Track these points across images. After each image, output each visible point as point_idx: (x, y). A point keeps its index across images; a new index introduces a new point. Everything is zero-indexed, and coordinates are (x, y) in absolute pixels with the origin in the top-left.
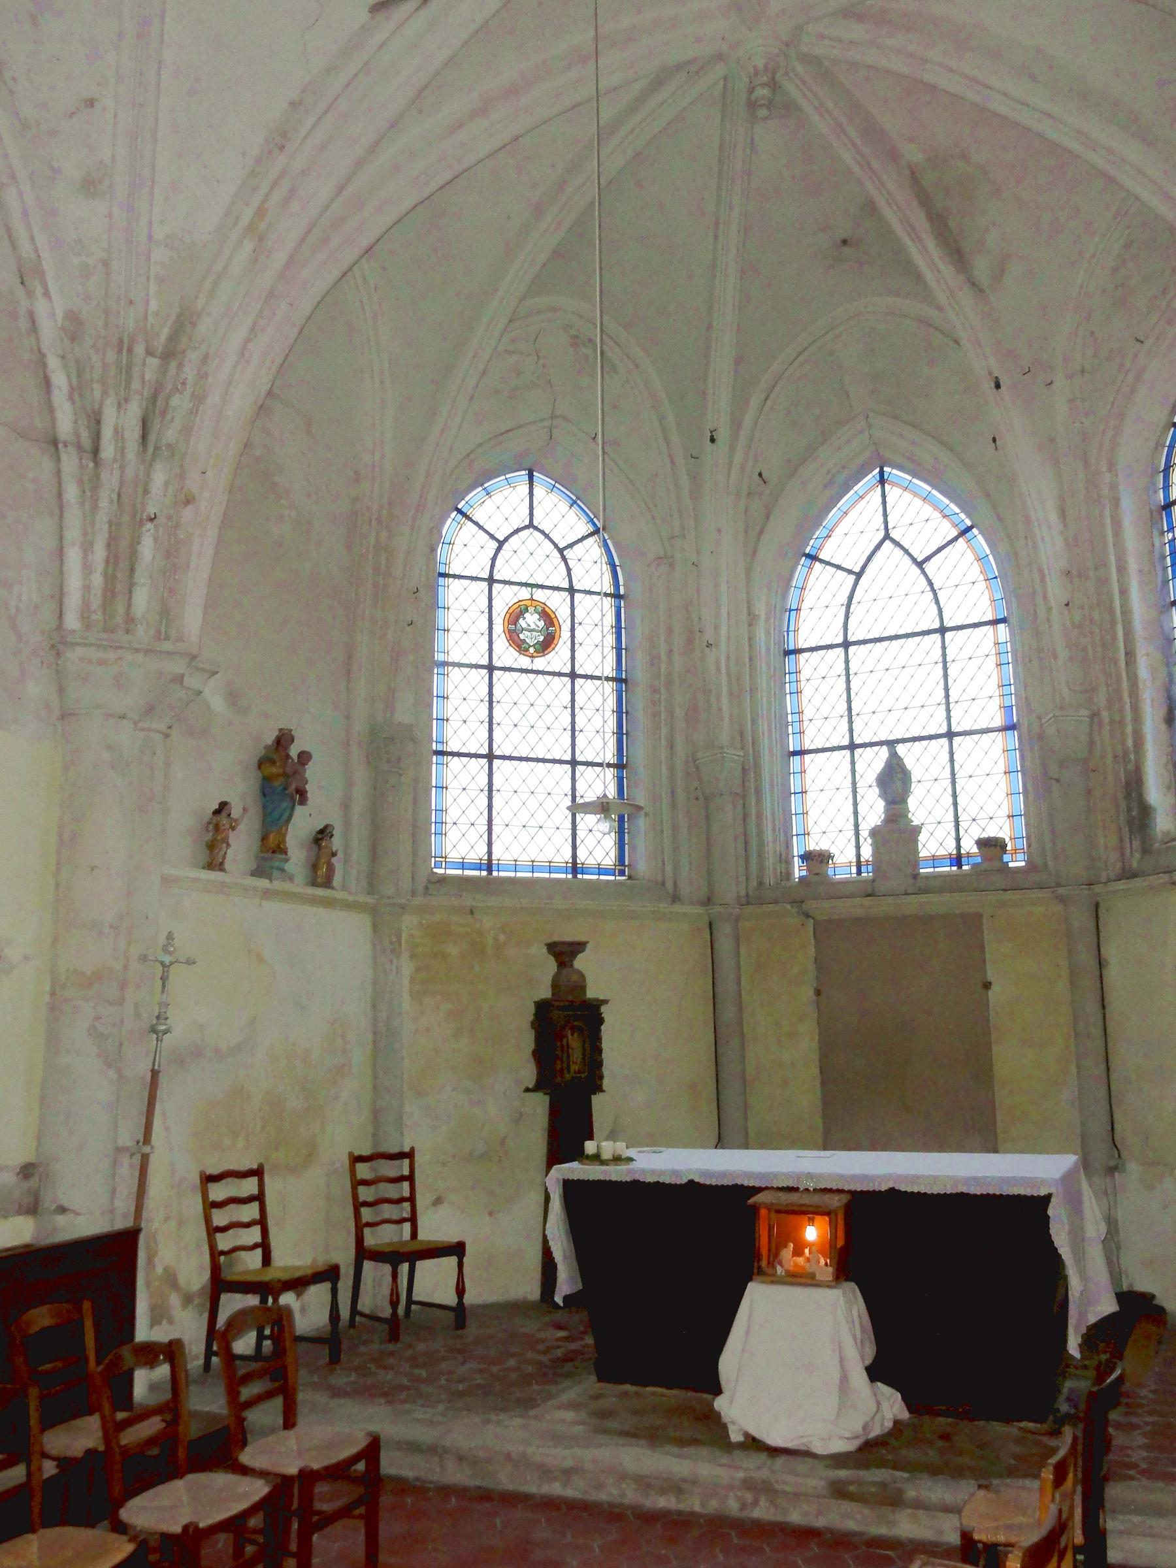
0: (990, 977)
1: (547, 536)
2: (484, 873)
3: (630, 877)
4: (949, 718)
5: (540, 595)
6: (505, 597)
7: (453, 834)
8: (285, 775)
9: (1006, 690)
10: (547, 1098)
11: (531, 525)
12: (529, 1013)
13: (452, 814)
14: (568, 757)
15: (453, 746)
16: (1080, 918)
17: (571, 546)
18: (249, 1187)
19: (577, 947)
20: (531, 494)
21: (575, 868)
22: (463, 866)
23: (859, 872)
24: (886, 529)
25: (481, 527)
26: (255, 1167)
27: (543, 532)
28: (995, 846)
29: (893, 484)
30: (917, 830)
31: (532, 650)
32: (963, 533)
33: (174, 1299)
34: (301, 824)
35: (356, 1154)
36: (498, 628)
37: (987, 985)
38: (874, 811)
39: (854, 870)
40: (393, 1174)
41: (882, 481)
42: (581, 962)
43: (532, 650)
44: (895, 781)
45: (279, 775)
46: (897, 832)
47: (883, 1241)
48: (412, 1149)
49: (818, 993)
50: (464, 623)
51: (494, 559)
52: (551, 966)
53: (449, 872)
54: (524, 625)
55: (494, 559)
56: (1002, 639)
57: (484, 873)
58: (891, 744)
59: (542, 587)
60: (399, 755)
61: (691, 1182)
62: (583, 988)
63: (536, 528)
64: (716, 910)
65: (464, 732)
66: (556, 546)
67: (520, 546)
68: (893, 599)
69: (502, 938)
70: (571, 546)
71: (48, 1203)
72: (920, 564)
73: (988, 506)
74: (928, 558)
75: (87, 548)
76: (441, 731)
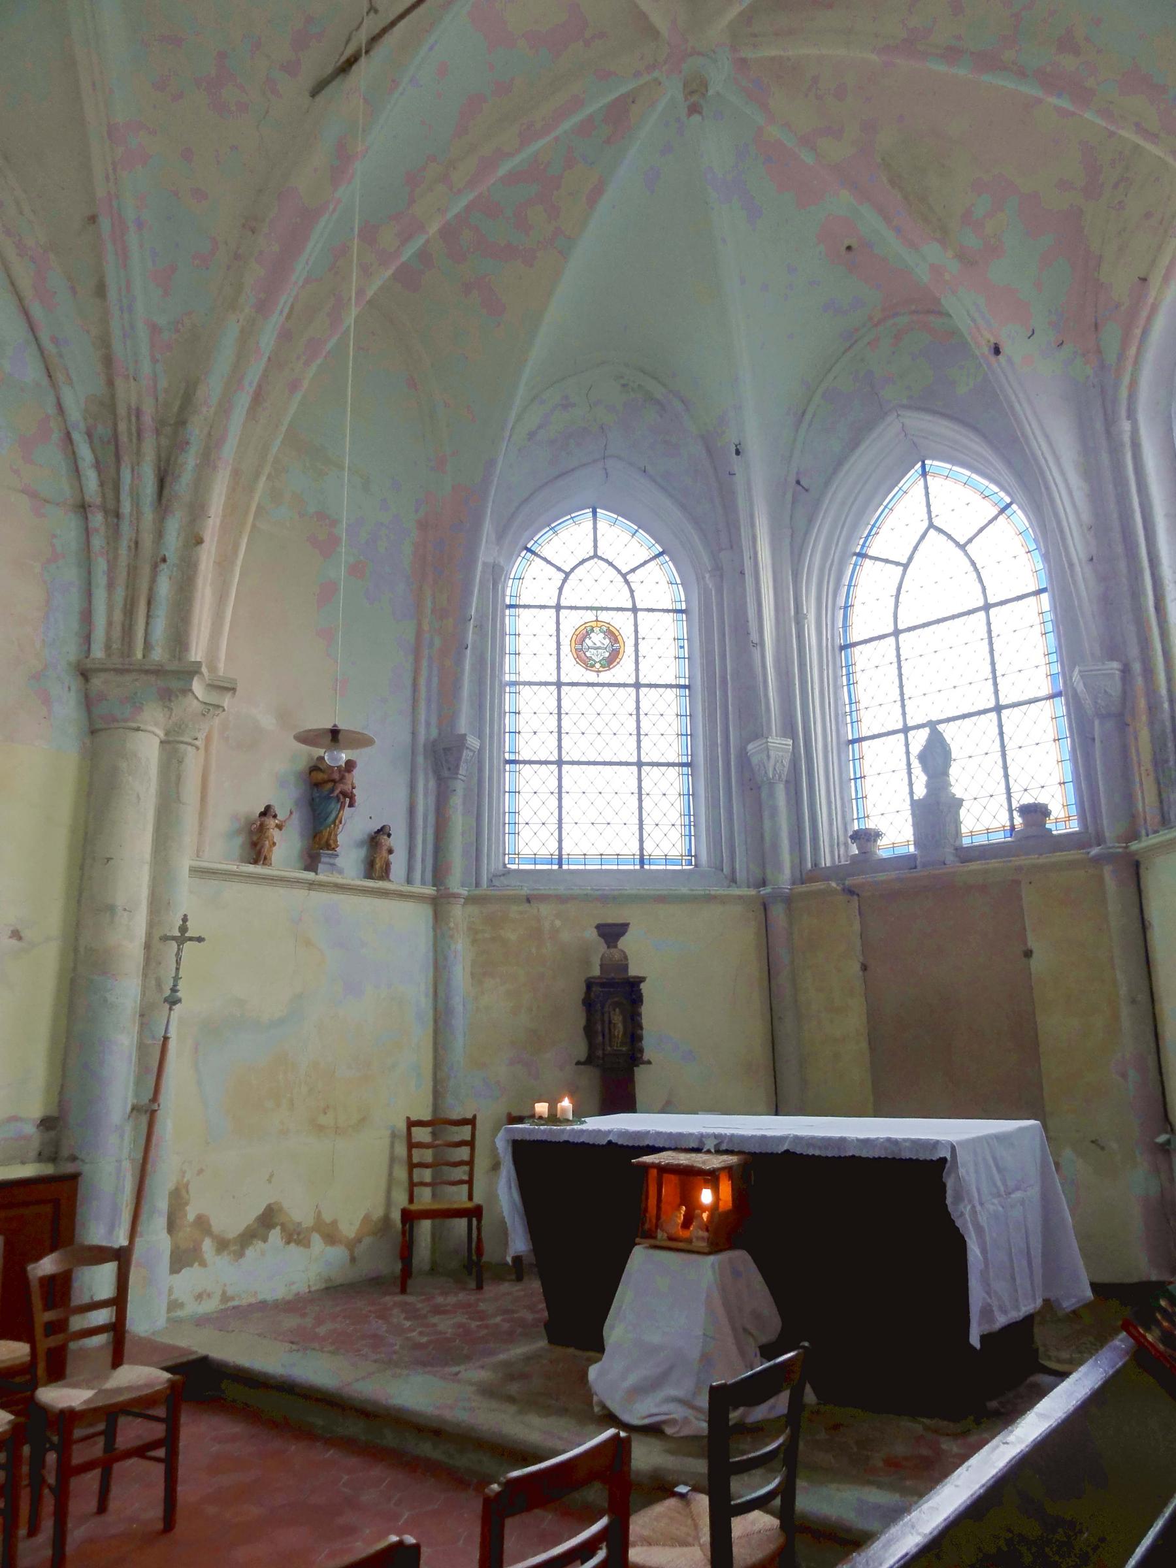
0: (1032, 943)
1: (611, 564)
2: (556, 867)
3: (696, 866)
4: (996, 692)
5: (604, 616)
6: (571, 622)
7: (525, 833)
11: (596, 556)
12: (579, 993)
13: (525, 815)
14: (635, 759)
15: (525, 755)
17: (633, 570)
24: (930, 518)
25: (549, 562)
27: (606, 561)
28: (1036, 811)
29: (935, 475)
30: (959, 803)
31: (598, 665)
32: (1002, 511)
33: (207, 1245)
34: (352, 827)
35: (414, 1118)
36: (566, 649)
37: (1028, 954)
41: (924, 474)
43: (598, 665)
44: (936, 757)
46: (936, 812)
48: (475, 1117)
49: (864, 968)
50: (531, 645)
51: (561, 589)
53: (522, 867)
54: (590, 644)
55: (561, 589)
57: (556, 867)
59: (607, 609)
60: (456, 761)
61: (610, 1142)
64: (767, 890)
65: (535, 741)
66: (619, 571)
68: (940, 582)
69: (558, 923)
70: (633, 570)
71: (65, 1153)
72: (963, 547)
73: (1026, 482)
74: (970, 541)
75: (111, 586)
76: (514, 743)
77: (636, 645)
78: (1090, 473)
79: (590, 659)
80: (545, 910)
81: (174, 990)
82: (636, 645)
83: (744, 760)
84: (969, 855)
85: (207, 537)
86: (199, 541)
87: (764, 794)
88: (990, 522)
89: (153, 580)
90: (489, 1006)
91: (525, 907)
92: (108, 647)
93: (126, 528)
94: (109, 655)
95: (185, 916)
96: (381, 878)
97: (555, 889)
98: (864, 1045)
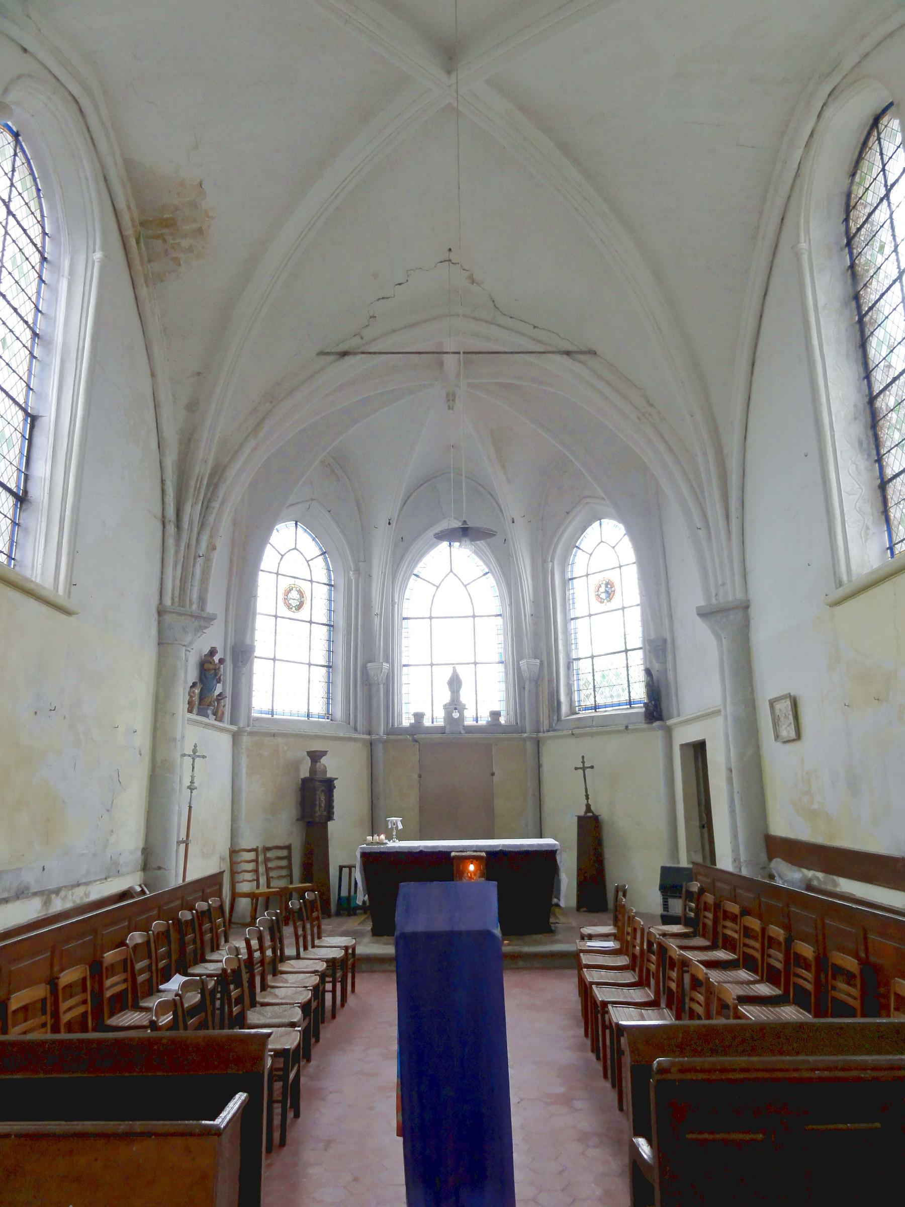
0: (494, 770)
6: (285, 583)
8: (215, 670)
10: (779, 860)
18: (284, 853)
19: (324, 753)
26: (287, 844)
37: (493, 774)
38: (444, 696)
42: (324, 760)
44: (455, 683)
46: (455, 705)
49: (420, 776)
50: (267, 592)
62: (325, 772)
67: (292, 559)
69: (286, 748)
72: (465, 586)
75: (175, 566)
78: (534, 577)
80: (280, 740)
81: (192, 782)
83: (364, 668)
84: (469, 730)
85: (219, 545)
86: (214, 548)
87: (374, 689)
89: (194, 566)
90: (257, 790)
92: (173, 599)
93: (185, 536)
96: (221, 720)
97: (274, 732)
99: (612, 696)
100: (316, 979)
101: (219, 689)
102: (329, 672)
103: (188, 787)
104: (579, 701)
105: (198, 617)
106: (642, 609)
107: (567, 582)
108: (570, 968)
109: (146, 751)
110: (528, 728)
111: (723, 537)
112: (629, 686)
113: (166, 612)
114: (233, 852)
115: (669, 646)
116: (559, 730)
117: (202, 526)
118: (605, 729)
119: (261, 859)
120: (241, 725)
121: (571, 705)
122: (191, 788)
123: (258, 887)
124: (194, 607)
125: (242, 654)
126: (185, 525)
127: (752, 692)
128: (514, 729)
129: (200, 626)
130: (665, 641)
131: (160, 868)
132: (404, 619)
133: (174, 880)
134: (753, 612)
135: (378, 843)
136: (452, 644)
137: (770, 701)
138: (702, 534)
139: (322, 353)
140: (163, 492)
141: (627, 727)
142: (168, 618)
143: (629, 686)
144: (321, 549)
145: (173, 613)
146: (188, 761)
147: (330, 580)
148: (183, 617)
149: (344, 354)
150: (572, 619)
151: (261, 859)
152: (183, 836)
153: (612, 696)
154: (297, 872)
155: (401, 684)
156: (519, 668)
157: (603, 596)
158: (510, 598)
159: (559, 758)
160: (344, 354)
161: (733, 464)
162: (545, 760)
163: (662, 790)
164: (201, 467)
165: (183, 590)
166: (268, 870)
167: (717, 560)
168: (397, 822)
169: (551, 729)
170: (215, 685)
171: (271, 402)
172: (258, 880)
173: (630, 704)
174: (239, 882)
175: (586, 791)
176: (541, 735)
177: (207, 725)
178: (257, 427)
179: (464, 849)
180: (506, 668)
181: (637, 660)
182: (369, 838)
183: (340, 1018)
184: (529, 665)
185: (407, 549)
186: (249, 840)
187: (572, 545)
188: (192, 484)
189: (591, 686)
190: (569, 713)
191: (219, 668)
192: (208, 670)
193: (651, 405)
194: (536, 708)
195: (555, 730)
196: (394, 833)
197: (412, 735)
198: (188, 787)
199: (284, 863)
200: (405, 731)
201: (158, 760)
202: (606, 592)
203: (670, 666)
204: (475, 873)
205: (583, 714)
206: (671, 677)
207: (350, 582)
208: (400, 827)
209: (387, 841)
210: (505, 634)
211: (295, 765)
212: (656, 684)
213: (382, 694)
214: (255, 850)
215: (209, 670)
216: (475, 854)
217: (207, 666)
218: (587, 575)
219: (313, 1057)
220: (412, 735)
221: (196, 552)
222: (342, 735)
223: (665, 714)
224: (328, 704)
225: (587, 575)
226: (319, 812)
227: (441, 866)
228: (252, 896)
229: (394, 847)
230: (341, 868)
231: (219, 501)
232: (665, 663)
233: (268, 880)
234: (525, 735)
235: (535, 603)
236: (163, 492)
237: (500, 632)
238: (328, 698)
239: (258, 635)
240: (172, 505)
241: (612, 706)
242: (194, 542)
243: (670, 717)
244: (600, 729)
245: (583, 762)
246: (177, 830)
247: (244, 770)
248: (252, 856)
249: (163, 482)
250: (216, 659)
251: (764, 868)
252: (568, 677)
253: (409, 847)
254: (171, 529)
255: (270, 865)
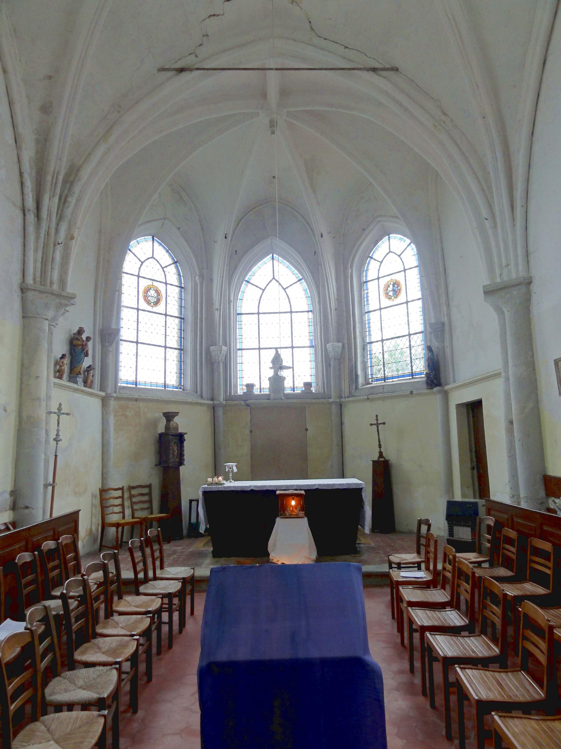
2: (134, 386)
5: (155, 284)
6: (144, 284)
8: (83, 345)
9: (311, 334)
11: (153, 257)
16: (334, 409)
17: (166, 267)
18: (146, 491)
19: (177, 414)
20: (153, 246)
21: (165, 386)
22: (127, 383)
23: (260, 392)
26: (148, 484)
31: (393, 298)
35: (131, 485)
37: (307, 430)
39: (259, 390)
40: (116, 496)
41: (273, 259)
42: (176, 419)
43: (393, 298)
45: (80, 345)
46: (277, 381)
47: (317, 505)
48: (123, 487)
49: (251, 432)
50: (129, 291)
51: (140, 268)
52: (164, 421)
55: (140, 268)
56: (310, 317)
57: (134, 386)
58: (276, 349)
62: (177, 428)
63: (154, 259)
67: (147, 263)
68: (274, 299)
69: (146, 410)
70: (166, 267)
72: (285, 289)
74: (287, 288)
75: (36, 251)
77: (166, 298)
79: (149, 300)
80: (141, 404)
81: (57, 435)
82: (166, 298)
83: (208, 352)
84: (288, 396)
87: (215, 366)
88: (294, 283)
89: (54, 251)
90: (122, 443)
91: (135, 403)
92: (34, 279)
93: (44, 226)
94: (35, 283)
95: (60, 403)
96: (90, 387)
97: (137, 397)
98: (249, 458)
99: (398, 370)
100: (146, 622)
101: (87, 362)
102: (181, 354)
103: (54, 439)
104: (372, 375)
105: (59, 296)
106: (423, 304)
107: (363, 284)
108: (380, 586)
109: (13, 407)
110: (333, 394)
111: (508, 224)
112: (411, 362)
113: (28, 289)
114: (103, 491)
115: (447, 328)
116: (357, 396)
117: (60, 218)
118: (394, 394)
119: (126, 495)
120: (109, 392)
121: (365, 377)
122: (57, 440)
123: (124, 518)
124: (55, 287)
125: (109, 336)
126: (44, 214)
127: (533, 356)
128: (322, 396)
129: (61, 304)
130: (443, 324)
131: (27, 508)
132: (238, 314)
133: (39, 516)
134: (534, 287)
135: (217, 484)
136: (275, 330)
137: (554, 361)
138: (487, 224)
139: (162, 69)
140: (22, 184)
141: (411, 392)
142: (30, 295)
143: (411, 362)
144: (173, 259)
145: (35, 290)
146: (54, 417)
147: (181, 283)
148: (44, 295)
149: (181, 70)
150: (366, 313)
151: (126, 495)
152: (51, 480)
153: (398, 370)
154: (156, 505)
155: (237, 363)
156: (326, 350)
157: (391, 293)
158: (319, 297)
159: (358, 418)
160: (181, 70)
161: (519, 160)
162: (346, 420)
163: (440, 439)
164: (57, 165)
165: (43, 272)
166: (132, 504)
167: (510, 238)
168: (233, 466)
169: (351, 395)
170: (85, 359)
171: (119, 112)
172: (123, 512)
173: (412, 376)
174: (107, 514)
175: (379, 442)
176: (343, 400)
177: (76, 390)
178: (108, 131)
179: (287, 488)
180: (315, 351)
181: (418, 341)
182: (210, 480)
183: (176, 648)
184: (334, 347)
185: (240, 260)
186: (117, 480)
187: (367, 256)
188: (49, 178)
189: (382, 363)
190: (364, 383)
191: (86, 344)
192: (76, 346)
193: (445, 114)
194: (339, 378)
195: (354, 396)
196: (231, 475)
197: (245, 401)
198: (54, 439)
199: (146, 498)
200: (240, 397)
201: (24, 415)
202: (394, 290)
203: (447, 344)
204: (296, 507)
205: (375, 384)
206: (448, 351)
207: (196, 284)
208: (235, 470)
209: (225, 482)
210: (315, 325)
211: (155, 423)
212: (435, 358)
213: (221, 371)
214: (122, 489)
215: (78, 345)
216: (296, 492)
217: (75, 342)
218: (378, 278)
219: (140, 706)
220: (245, 401)
221: (55, 240)
222: (190, 400)
223: (443, 381)
224: (180, 377)
225: (378, 278)
226: (173, 460)
227: (269, 505)
228: (117, 525)
229: (230, 487)
230: (191, 501)
231: (75, 196)
232: (443, 341)
233: (133, 511)
234: (331, 400)
235: (339, 300)
236: (22, 184)
237: (311, 324)
238: (180, 374)
239: (123, 323)
240: (31, 195)
241: (398, 377)
242: (53, 231)
243: (447, 384)
244: (389, 394)
245: (377, 420)
246: (42, 474)
247: (112, 427)
248: (119, 493)
249: (21, 174)
250: (84, 337)
251: (542, 503)
252: (364, 356)
253: (242, 487)
254: (31, 217)
255: (134, 500)
